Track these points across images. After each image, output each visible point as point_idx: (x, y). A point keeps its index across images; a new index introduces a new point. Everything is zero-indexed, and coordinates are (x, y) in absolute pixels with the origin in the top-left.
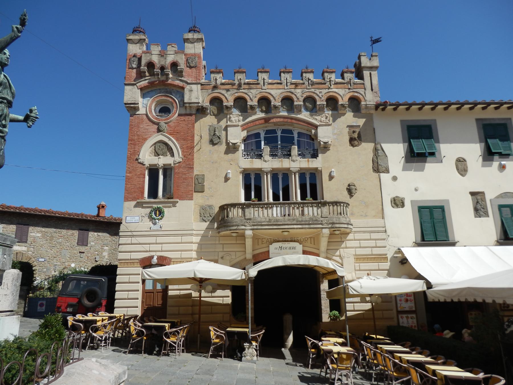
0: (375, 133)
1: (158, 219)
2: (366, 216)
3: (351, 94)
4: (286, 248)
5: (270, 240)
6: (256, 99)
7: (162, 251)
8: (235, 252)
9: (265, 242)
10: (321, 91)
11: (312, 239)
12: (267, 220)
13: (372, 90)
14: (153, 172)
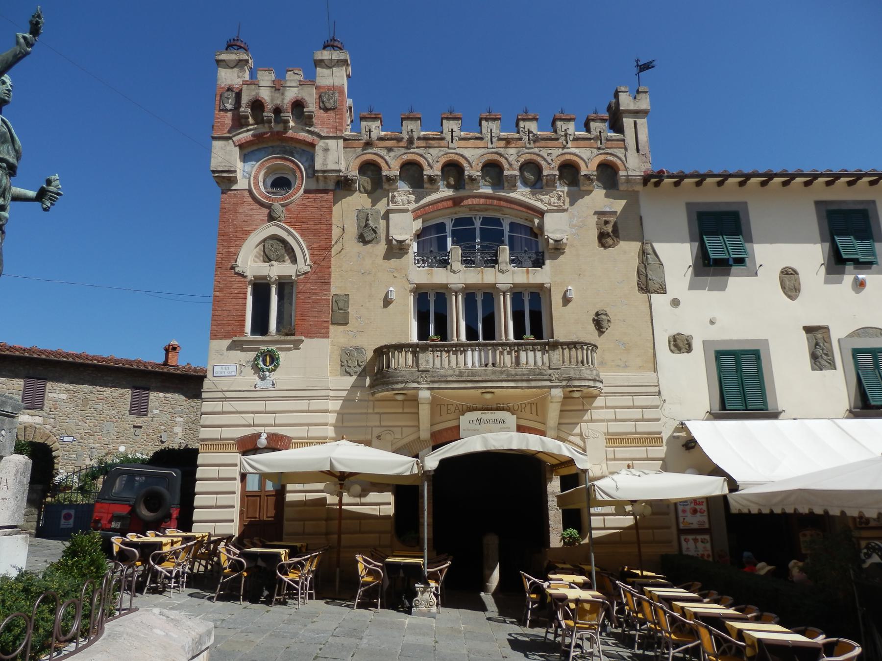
0: (641, 224)
2: (626, 366)
3: (602, 157)
4: (488, 421)
5: (460, 407)
6: (439, 166)
7: (275, 425)
8: (401, 427)
10: (550, 151)
11: (534, 407)
12: (457, 373)
13: (638, 150)
14: (261, 289)
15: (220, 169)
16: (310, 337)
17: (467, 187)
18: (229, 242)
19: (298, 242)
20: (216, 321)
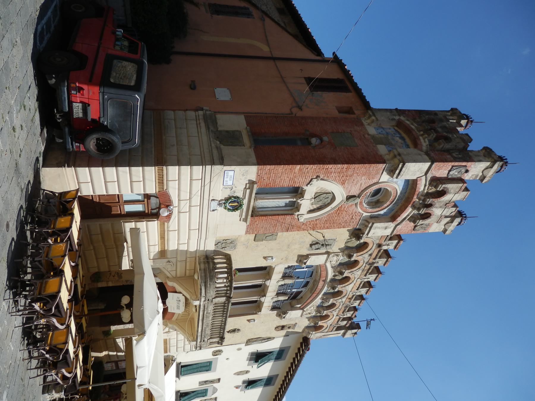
8: (176, 270)
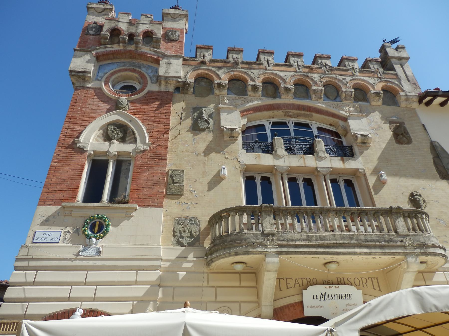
0: (425, 129)
1: (96, 238)
4: (333, 297)
5: (300, 281)
6: (260, 80)
7: (94, 299)
8: (240, 303)
9: (292, 284)
10: (344, 77)
11: (375, 282)
12: (304, 237)
13: (409, 81)
14: (98, 168)
15: (76, 70)
16: (144, 206)
17: (283, 96)
18: (75, 124)
19: (140, 127)
20: (47, 187)
